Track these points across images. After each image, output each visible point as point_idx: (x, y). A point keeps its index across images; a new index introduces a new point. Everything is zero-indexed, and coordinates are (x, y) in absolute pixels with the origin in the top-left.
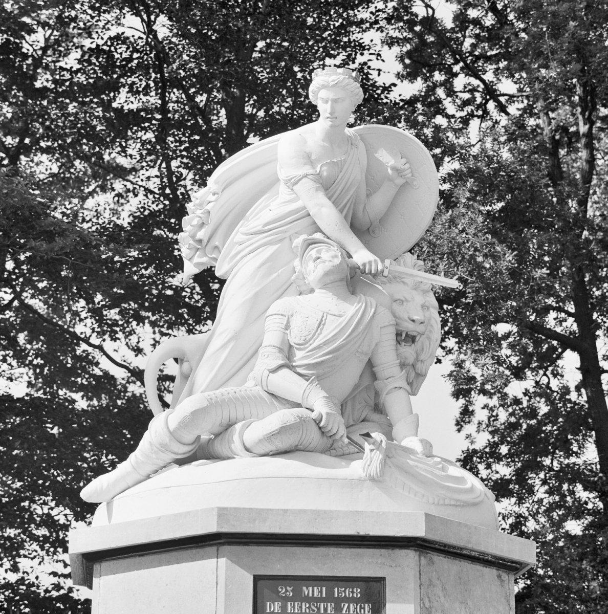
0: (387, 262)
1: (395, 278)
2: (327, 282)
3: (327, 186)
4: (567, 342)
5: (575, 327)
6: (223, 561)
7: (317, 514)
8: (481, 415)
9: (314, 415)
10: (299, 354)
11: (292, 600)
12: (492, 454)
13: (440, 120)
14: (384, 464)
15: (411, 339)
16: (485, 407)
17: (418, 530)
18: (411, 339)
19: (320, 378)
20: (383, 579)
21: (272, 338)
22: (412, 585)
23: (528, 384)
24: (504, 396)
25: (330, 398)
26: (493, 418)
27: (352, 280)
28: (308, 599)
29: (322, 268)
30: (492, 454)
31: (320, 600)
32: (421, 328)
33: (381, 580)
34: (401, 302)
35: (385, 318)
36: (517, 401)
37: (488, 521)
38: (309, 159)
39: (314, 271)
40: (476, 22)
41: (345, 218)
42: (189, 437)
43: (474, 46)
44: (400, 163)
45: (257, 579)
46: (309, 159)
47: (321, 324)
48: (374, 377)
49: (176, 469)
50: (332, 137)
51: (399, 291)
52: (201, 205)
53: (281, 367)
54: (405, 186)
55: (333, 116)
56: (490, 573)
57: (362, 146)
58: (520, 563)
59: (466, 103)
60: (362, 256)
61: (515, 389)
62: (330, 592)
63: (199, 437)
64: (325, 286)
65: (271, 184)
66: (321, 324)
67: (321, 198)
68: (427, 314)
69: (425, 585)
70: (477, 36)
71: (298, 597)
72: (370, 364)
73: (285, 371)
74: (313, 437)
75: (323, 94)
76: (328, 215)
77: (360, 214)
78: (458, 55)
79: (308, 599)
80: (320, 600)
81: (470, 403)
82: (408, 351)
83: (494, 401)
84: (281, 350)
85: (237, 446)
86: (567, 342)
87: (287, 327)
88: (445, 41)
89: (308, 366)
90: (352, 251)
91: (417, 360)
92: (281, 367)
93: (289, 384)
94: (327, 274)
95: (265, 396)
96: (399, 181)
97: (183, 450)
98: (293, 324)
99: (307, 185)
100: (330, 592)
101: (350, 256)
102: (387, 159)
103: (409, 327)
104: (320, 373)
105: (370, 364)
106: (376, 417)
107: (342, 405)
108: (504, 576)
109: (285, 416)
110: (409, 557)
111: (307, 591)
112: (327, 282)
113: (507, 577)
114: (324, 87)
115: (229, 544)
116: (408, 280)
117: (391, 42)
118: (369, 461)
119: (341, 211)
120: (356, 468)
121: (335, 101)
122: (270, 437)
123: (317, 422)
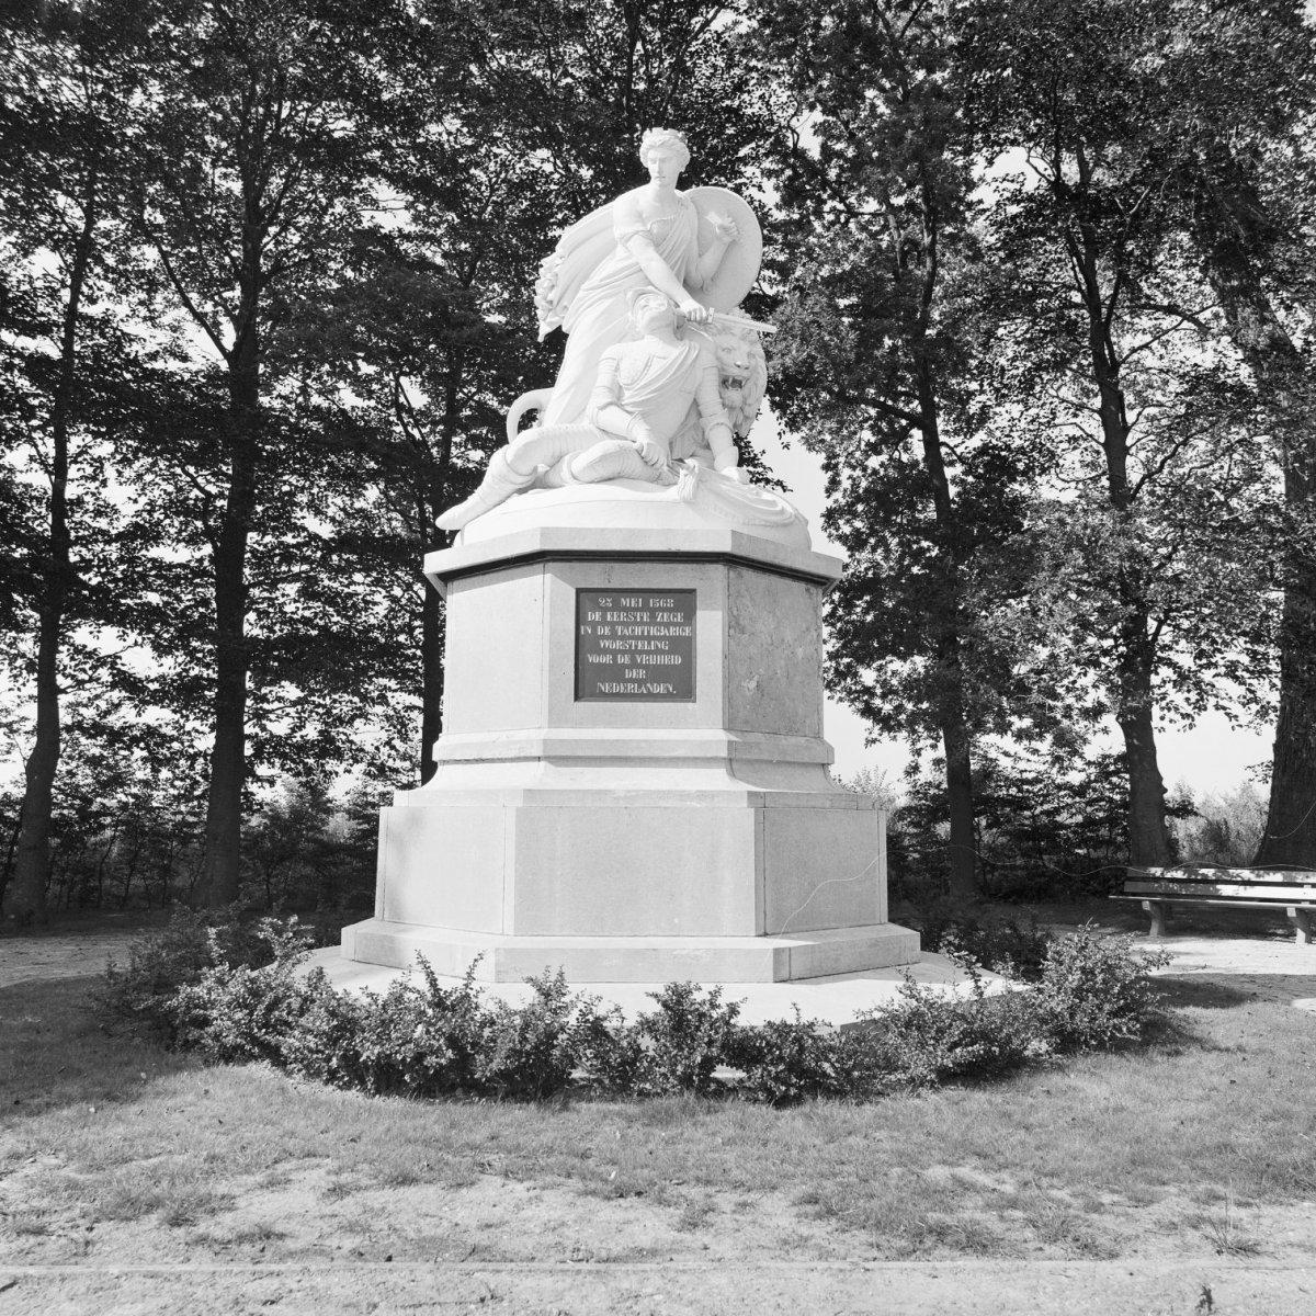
0: (712, 310)
1: (725, 330)
2: (655, 327)
3: (657, 243)
4: (915, 421)
5: (919, 409)
6: (548, 576)
7: (632, 532)
8: (846, 484)
9: (635, 446)
10: (627, 394)
11: (612, 609)
12: (849, 511)
13: (812, 240)
14: (697, 487)
15: (737, 384)
16: (850, 477)
17: (725, 546)
18: (737, 384)
19: (645, 416)
20: (694, 591)
21: (604, 378)
22: (721, 597)
23: (884, 458)
24: (865, 469)
25: (652, 431)
26: (855, 485)
27: (681, 327)
28: (626, 609)
29: (648, 315)
30: (849, 511)
31: (637, 609)
32: (746, 374)
33: (692, 591)
34: (729, 350)
35: (708, 359)
36: (875, 472)
37: (828, 553)
38: (640, 217)
39: (642, 318)
40: (840, 155)
41: (677, 275)
42: (526, 468)
43: (839, 176)
44: (727, 222)
45: (579, 592)
46: (640, 217)
47: (647, 366)
48: (700, 415)
49: (516, 497)
50: (661, 198)
51: (726, 341)
52: (550, 269)
53: (611, 404)
54: (733, 243)
55: (661, 176)
56: (802, 586)
57: (692, 207)
58: (828, 579)
59: (832, 223)
60: (688, 305)
61: (874, 462)
62: (646, 603)
63: (535, 469)
64: (652, 332)
65: (609, 249)
66: (647, 366)
67: (651, 252)
68: (753, 362)
69: (732, 595)
70: (841, 167)
71: (617, 607)
72: (695, 403)
73: (613, 408)
74: (636, 465)
75: (652, 154)
76: (656, 268)
77: (693, 274)
78: (825, 184)
79: (626, 609)
80: (637, 609)
81: (838, 474)
82: (734, 395)
83: (858, 473)
84: (611, 390)
85: (565, 474)
86: (915, 421)
87: (617, 369)
88: (815, 170)
89: (635, 404)
90: (678, 300)
91: (745, 403)
92: (611, 404)
93: (616, 419)
94: (653, 319)
95: (597, 432)
96: (727, 240)
97: (521, 481)
98: (622, 366)
99: (637, 241)
100: (646, 603)
101: (677, 306)
102: (715, 219)
103: (734, 372)
104: (646, 411)
105: (695, 403)
106: (701, 452)
107: (671, 444)
108: (813, 590)
109: (609, 445)
110: (718, 571)
111: (625, 602)
112: (655, 327)
113: (817, 592)
114: (652, 147)
115: (554, 561)
116: (737, 331)
117: (769, 174)
118: (686, 482)
119: (672, 268)
120: (672, 493)
121: (662, 161)
122: (592, 465)
123: (639, 452)
